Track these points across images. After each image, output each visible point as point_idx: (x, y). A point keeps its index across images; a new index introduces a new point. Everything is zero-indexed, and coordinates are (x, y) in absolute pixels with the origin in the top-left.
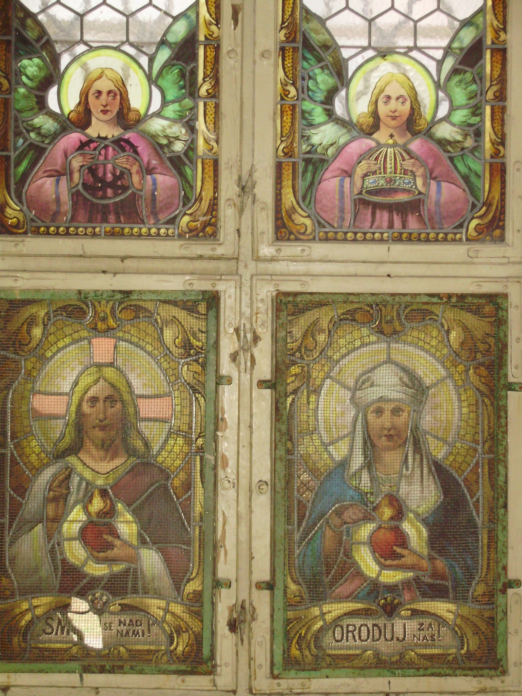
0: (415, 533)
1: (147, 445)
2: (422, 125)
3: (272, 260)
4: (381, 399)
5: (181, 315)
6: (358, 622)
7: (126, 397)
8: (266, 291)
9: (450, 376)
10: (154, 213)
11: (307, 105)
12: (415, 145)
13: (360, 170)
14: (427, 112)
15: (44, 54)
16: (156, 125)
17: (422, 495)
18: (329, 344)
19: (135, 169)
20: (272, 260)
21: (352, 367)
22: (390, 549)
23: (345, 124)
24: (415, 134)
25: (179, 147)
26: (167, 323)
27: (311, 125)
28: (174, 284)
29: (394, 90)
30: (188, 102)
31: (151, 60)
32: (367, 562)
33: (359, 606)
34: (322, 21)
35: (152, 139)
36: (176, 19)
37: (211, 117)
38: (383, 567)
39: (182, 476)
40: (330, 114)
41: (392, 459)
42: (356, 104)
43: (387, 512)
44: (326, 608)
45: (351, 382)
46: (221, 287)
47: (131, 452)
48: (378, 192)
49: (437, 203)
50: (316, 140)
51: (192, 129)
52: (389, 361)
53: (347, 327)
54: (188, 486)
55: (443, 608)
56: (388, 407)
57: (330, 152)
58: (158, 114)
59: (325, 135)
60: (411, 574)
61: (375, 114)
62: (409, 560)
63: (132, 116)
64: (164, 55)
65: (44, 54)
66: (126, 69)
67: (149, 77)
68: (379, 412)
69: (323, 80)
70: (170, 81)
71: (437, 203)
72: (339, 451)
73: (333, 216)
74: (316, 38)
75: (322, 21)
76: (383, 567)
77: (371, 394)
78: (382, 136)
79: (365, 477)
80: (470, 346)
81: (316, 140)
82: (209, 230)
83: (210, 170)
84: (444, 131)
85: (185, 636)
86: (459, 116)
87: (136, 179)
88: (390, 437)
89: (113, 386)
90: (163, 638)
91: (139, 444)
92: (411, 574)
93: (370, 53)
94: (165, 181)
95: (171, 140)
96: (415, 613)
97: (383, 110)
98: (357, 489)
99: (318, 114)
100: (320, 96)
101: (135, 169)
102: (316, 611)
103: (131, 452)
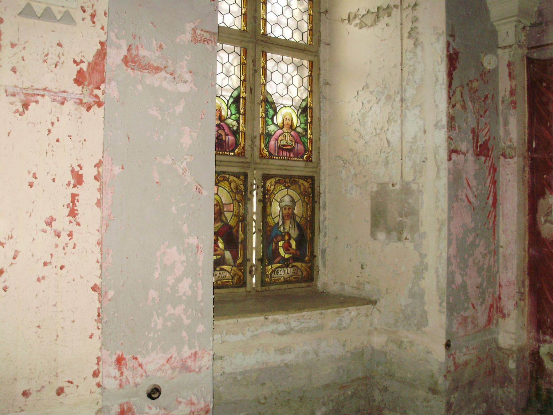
0: (293, 244)
1: (227, 220)
2: (294, 128)
3: (260, 164)
4: (286, 205)
5: (236, 179)
6: (280, 269)
7: (221, 204)
8: (260, 173)
9: (300, 198)
10: (229, 148)
11: (267, 119)
12: (292, 133)
13: (280, 139)
14: (295, 123)
15: (156, 275)
16: (229, 121)
17: (294, 233)
18: (274, 189)
19: (223, 134)
20: (260, 164)
21: (278, 196)
22: (287, 248)
23: (277, 125)
24: (292, 130)
25: (235, 128)
26: (232, 182)
27: (268, 125)
28: (236, 170)
29: (288, 117)
30: (237, 115)
31: (228, 101)
32: (281, 251)
33: (280, 265)
34: (271, 95)
35: (228, 125)
36: (235, 90)
37: (243, 120)
38: (286, 253)
39: (236, 228)
40: (273, 123)
41: (288, 222)
42: (279, 119)
43: (287, 238)
44: (273, 266)
45: (279, 201)
46: (248, 171)
47: (222, 221)
48: (284, 145)
49: (297, 150)
50: (269, 129)
51: (239, 124)
52: (287, 194)
53: (278, 184)
54: (238, 231)
55: (298, 264)
56: (287, 208)
57: (273, 133)
58: (230, 118)
59: (272, 128)
60: (291, 255)
61: (283, 123)
62: (291, 251)
63: (223, 118)
64: (231, 100)
65: (156, 275)
66: (221, 103)
67: (227, 106)
68: (285, 209)
69: (271, 112)
70: (233, 109)
71: (297, 150)
72: (276, 220)
73: (272, 152)
74: (270, 100)
75: (271, 95)
76: (286, 253)
77: (283, 204)
78: (285, 129)
79: (282, 228)
80: (238, 190)
81: (269, 129)
82: (243, 154)
83: (243, 136)
84: (299, 130)
85: (237, 276)
86: (302, 126)
87: (224, 137)
88: (288, 216)
89: (217, 201)
90: (231, 278)
91: (224, 219)
92: (291, 255)
93: (282, 106)
94: (231, 138)
95: (234, 126)
96: (293, 266)
97: (285, 122)
98: (280, 231)
99: (270, 122)
100: (270, 117)
101: (223, 134)
102: (270, 267)
103: (222, 221)
